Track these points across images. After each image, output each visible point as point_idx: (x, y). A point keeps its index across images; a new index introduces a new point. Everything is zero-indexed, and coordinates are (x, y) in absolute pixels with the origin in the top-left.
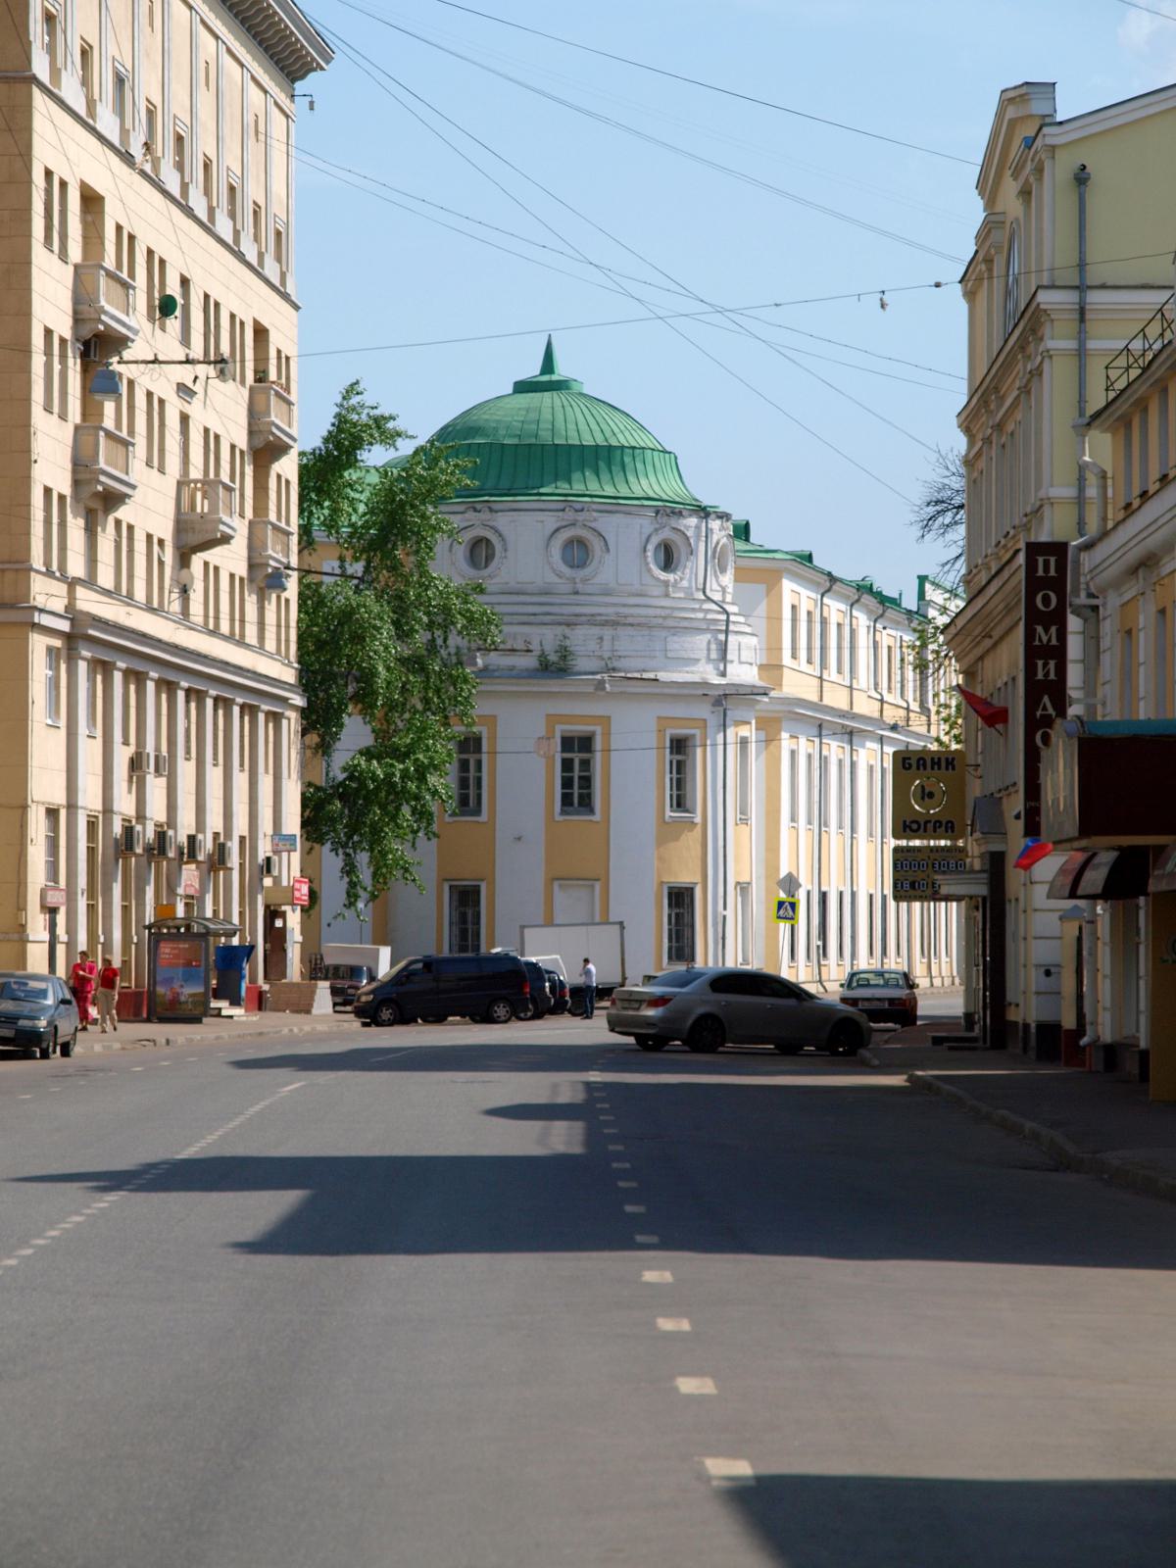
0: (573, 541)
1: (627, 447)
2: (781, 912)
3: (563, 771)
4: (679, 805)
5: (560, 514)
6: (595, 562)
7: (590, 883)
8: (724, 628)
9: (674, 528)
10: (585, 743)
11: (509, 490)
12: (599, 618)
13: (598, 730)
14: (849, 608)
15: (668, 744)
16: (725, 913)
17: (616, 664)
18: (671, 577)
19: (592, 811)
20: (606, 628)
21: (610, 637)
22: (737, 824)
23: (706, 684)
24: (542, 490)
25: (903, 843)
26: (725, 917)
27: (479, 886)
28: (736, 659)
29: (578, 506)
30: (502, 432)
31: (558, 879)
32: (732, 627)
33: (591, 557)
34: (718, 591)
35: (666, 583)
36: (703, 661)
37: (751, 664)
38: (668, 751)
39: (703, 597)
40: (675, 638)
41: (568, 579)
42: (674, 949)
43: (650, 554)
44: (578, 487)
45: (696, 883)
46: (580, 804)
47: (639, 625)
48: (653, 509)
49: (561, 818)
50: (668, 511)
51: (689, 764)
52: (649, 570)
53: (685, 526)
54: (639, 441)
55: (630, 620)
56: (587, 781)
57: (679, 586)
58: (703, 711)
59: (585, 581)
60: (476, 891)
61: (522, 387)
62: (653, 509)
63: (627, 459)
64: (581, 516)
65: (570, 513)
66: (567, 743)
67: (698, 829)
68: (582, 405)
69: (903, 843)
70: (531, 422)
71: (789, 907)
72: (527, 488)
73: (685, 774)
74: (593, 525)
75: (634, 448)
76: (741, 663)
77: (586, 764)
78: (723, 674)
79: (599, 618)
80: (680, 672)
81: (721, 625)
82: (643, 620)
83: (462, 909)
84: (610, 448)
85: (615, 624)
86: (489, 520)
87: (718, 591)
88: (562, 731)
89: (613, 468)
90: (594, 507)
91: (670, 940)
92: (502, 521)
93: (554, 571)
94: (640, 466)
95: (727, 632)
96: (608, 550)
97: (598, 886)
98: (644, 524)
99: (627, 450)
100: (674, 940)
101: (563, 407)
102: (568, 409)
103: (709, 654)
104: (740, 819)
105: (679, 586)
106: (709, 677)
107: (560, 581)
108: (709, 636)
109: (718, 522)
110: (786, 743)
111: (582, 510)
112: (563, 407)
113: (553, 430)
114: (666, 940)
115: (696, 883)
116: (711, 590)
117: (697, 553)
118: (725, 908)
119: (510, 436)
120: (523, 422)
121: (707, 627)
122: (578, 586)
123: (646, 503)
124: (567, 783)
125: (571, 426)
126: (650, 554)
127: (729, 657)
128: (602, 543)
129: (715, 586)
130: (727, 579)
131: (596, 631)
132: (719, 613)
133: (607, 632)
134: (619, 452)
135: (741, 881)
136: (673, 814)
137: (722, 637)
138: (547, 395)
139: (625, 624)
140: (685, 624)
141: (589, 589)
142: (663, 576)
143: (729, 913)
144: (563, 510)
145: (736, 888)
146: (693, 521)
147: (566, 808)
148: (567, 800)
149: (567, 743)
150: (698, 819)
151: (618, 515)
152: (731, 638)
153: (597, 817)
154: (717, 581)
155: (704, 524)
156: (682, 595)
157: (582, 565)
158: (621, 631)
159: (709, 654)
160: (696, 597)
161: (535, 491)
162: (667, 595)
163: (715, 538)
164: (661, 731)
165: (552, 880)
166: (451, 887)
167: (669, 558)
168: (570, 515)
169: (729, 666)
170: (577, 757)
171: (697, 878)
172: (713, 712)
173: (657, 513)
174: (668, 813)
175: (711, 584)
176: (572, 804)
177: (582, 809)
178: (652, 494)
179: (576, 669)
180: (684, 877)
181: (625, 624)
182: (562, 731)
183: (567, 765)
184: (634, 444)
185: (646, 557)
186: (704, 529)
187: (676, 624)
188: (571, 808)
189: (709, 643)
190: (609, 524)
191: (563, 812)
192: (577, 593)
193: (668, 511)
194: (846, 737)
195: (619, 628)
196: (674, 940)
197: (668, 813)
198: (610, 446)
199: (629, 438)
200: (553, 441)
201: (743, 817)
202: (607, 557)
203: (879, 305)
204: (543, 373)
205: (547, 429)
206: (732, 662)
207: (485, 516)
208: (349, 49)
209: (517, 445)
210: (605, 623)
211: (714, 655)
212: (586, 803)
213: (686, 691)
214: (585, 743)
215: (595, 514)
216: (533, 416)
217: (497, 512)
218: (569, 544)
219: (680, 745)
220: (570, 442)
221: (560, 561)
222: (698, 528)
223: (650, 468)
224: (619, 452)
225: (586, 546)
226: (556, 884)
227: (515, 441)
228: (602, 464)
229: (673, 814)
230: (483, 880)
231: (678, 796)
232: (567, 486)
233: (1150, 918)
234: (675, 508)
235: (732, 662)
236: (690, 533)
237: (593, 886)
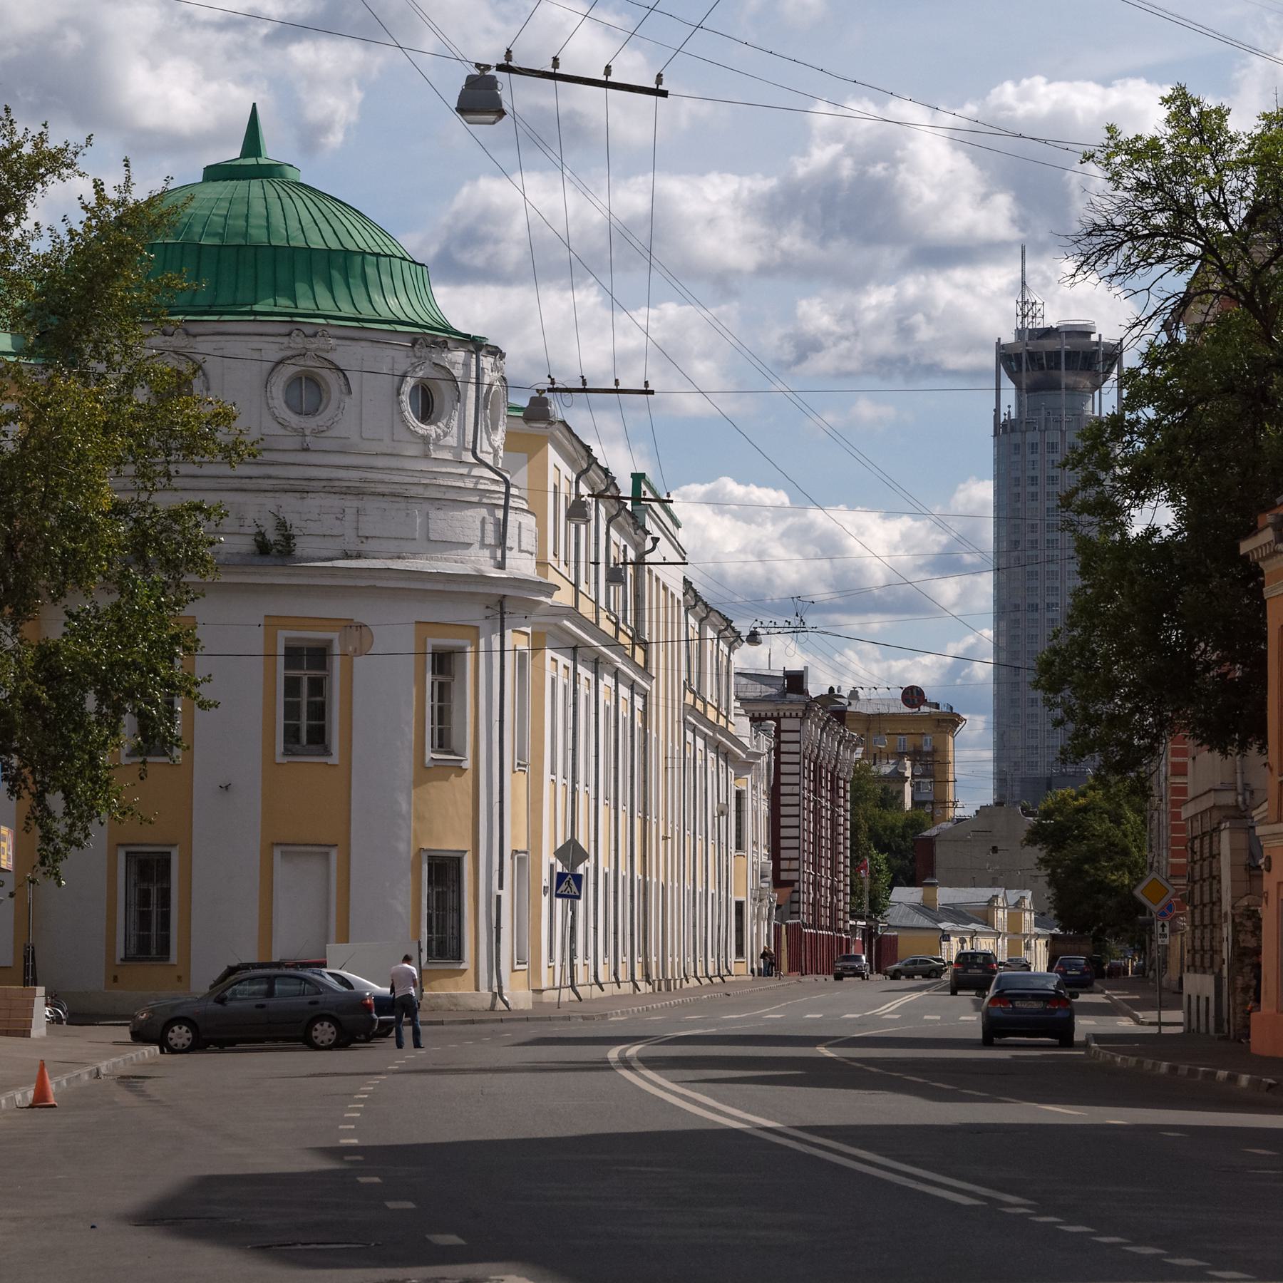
0: (301, 378)
1: (369, 254)
2: (563, 887)
3: (286, 695)
4: (440, 746)
5: (285, 340)
6: (333, 404)
7: (326, 849)
8: (502, 502)
9: (436, 364)
10: (319, 655)
11: (210, 306)
12: (337, 483)
13: (280, 759)
14: (574, 476)
15: (281, 651)
16: (500, 892)
17: (364, 547)
18: (430, 430)
19: (327, 752)
20: (349, 497)
21: (354, 511)
22: (514, 772)
23: (481, 579)
24: (257, 308)
25: (295, 699)
26: (499, 897)
27: (170, 853)
28: (515, 546)
29: (308, 330)
30: (197, 229)
31: (278, 844)
32: (511, 504)
33: (325, 401)
34: (490, 453)
35: (425, 439)
36: (477, 545)
37: (532, 554)
38: (281, 661)
39: (474, 461)
40: (441, 514)
41: (295, 430)
42: (434, 943)
43: (405, 398)
44: (305, 304)
45: (465, 852)
46: (310, 742)
47: (393, 495)
48: (410, 338)
49: (285, 760)
50: (429, 339)
51: (455, 686)
52: (404, 421)
53: (451, 363)
54: (371, 242)
55: (382, 488)
56: (319, 711)
57: (442, 443)
58: (473, 614)
59: (317, 432)
60: (165, 860)
61: (215, 173)
62: (410, 338)
63: (370, 271)
64: (314, 344)
65: (298, 339)
66: (294, 655)
67: (468, 776)
68: (303, 196)
69: (295, 699)
70: (237, 217)
71: (572, 882)
72: (234, 305)
73: (450, 701)
74: (329, 356)
75: (378, 255)
76: (521, 551)
77: (317, 686)
78: (501, 566)
79: (337, 483)
80: (446, 560)
81: (499, 498)
82: (397, 489)
83: (144, 886)
84: (347, 253)
85: (359, 493)
86: (185, 347)
87: (490, 453)
88: (287, 639)
89: (351, 281)
90: (332, 331)
91: (430, 931)
92: (203, 346)
93: (276, 418)
94: (386, 280)
95: (506, 507)
96: (350, 392)
97: (334, 854)
98: (397, 358)
99: (369, 257)
100: (434, 930)
101: (279, 198)
102: (286, 201)
103: (483, 537)
104: (519, 764)
105: (442, 443)
106: (483, 568)
107: (282, 432)
108: (484, 512)
109: (491, 359)
110: (549, 653)
111: (315, 335)
112: (279, 198)
113: (268, 228)
114: (425, 930)
115: (465, 852)
116: (482, 452)
117: (465, 400)
118: (501, 887)
119: (208, 235)
120: (226, 217)
121: (480, 499)
122: (308, 439)
123: (400, 328)
124: (291, 711)
125: (293, 224)
126: (405, 398)
127: (509, 543)
128: (342, 381)
129: (486, 447)
130: (499, 438)
131: (335, 501)
132: (497, 481)
133: (351, 503)
134: (358, 259)
135: (519, 849)
136: (436, 756)
137: (500, 514)
138: (255, 183)
139: (373, 494)
140: (451, 495)
141: (325, 444)
142: (422, 429)
143: (506, 895)
144: (289, 335)
145: (512, 858)
146: (459, 356)
147: (290, 746)
148: (292, 734)
149: (294, 655)
150: (467, 764)
151: (363, 344)
152: (512, 517)
153: (334, 760)
154: (489, 439)
155: (474, 361)
156: (448, 456)
157: (314, 411)
158: (370, 504)
159: (483, 537)
160: (464, 459)
161: (247, 308)
162: (426, 456)
163: (487, 380)
164: (271, 639)
165: (272, 845)
166: (127, 854)
167: (427, 408)
168: (298, 342)
169: (508, 553)
170: (305, 675)
171: (466, 845)
172: (487, 618)
173: (414, 342)
174: (430, 755)
175: (484, 445)
176: (298, 741)
177: (313, 747)
178: (403, 318)
179: (305, 553)
180: (450, 843)
181: (373, 494)
182: (287, 639)
183: (292, 686)
184: (377, 250)
185: (400, 403)
186: (474, 368)
187: (439, 496)
188: (1169, 832)
189: (483, 521)
190: (347, 355)
191: (287, 752)
192: (307, 450)
193: (429, 339)
194: (570, 651)
195: (365, 498)
196: (434, 930)
197: (430, 755)
198: (330, 249)
199: (371, 242)
200: (269, 242)
201: (521, 763)
202: (347, 400)
203: (131, 164)
204: (243, 156)
205: (259, 227)
206: (511, 549)
207: (178, 341)
208: (194, 480)
209: (239, 246)
210: (346, 492)
211: (490, 539)
212: (318, 737)
213: (454, 588)
214: (319, 655)
215: (332, 341)
216: (240, 209)
217: (195, 336)
218: (296, 380)
219: (444, 662)
220: (293, 243)
221: (284, 406)
222: (466, 365)
223: (399, 284)
224: (358, 259)
225: (318, 386)
226: (277, 852)
227: (216, 241)
228: (336, 276)
229: (436, 756)
230: (174, 845)
231: (440, 731)
232: (288, 303)
233: (1006, 1099)
234: (437, 336)
235: (511, 549)
236: (458, 372)
237: (327, 853)
